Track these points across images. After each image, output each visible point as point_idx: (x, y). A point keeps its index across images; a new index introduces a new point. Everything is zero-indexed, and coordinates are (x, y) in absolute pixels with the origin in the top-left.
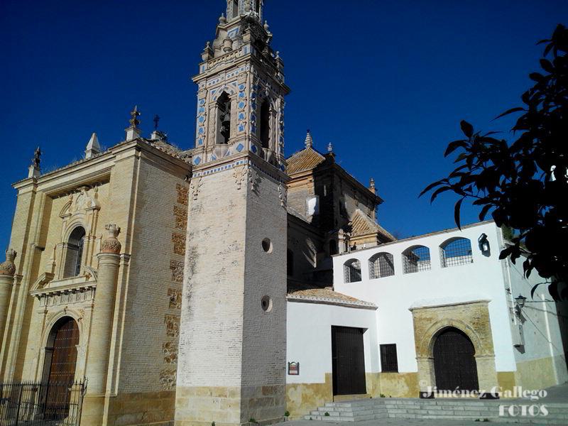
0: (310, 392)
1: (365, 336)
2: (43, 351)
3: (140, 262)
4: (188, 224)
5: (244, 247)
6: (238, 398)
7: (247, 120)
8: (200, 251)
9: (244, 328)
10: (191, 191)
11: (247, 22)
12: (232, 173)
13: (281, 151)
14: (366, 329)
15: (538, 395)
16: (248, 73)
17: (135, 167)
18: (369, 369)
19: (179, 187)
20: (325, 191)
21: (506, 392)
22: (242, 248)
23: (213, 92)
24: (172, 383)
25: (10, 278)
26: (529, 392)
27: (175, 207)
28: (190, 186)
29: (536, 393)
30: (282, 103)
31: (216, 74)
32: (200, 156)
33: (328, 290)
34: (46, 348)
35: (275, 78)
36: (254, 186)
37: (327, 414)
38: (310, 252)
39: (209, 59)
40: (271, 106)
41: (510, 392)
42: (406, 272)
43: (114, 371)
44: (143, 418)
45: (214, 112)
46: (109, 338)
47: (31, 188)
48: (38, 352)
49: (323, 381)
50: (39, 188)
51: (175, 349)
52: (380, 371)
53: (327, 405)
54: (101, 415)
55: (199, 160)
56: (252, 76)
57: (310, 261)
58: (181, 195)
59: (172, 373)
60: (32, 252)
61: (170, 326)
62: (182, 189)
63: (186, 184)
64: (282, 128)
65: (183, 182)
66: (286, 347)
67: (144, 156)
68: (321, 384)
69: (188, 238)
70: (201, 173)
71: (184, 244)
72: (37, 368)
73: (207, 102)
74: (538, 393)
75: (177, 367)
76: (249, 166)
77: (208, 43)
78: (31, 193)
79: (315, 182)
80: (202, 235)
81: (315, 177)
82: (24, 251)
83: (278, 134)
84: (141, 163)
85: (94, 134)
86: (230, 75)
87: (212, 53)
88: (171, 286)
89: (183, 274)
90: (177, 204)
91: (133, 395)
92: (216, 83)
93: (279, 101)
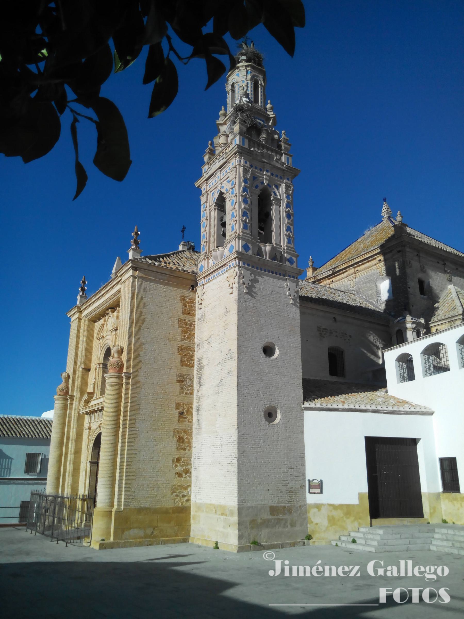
0: (338, 514)
1: (420, 447)
2: (89, 465)
3: (142, 378)
4: (196, 335)
5: (237, 356)
6: (235, 519)
7: (237, 219)
8: (205, 362)
9: (239, 443)
10: (197, 300)
11: (239, 109)
12: (226, 277)
13: (289, 242)
14: (419, 439)
15: (435, 573)
16: (237, 167)
17: (133, 286)
18: (424, 488)
19: (183, 299)
20: (397, 270)
21: (389, 568)
22: (235, 357)
23: (213, 194)
24: (186, 498)
25: (64, 399)
26: (422, 569)
27: (180, 320)
28: (197, 296)
29: (433, 570)
30: (287, 188)
31: (212, 175)
32: (203, 263)
33: (380, 393)
34: (90, 462)
35: (274, 163)
36: (246, 287)
37: (354, 541)
38: (371, 345)
39: (210, 158)
40: (273, 194)
41: (395, 568)
42: (426, 375)
43: (120, 486)
44: (153, 533)
45: (214, 214)
46: (115, 455)
47: (77, 315)
48: (85, 465)
49: (355, 501)
50: (84, 314)
51: (188, 463)
52: (441, 489)
53: (362, 530)
54: (109, 528)
55: (202, 267)
56: (241, 169)
57: (372, 357)
58: (186, 306)
59: (186, 488)
60: (80, 374)
61: (180, 440)
62: (187, 300)
63: (192, 295)
64: (289, 216)
65: (187, 293)
66: (305, 462)
67: (141, 275)
68: (353, 505)
69: (196, 349)
70: (203, 281)
71: (193, 356)
72: (85, 480)
73: (208, 206)
74: (436, 570)
75: (190, 482)
76: (239, 267)
77: (210, 142)
78: (77, 320)
79: (385, 260)
80: (205, 344)
81: (384, 255)
82: (74, 373)
83: (284, 223)
84: (138, 281)
85: (117, 258)
86: (225, 172)
87: (212, 153)
88: (180, 400)
89: (192, 386)
90: (182, 317)
91: (140, 511)
92: (214, 184)
93: (283, 187)
